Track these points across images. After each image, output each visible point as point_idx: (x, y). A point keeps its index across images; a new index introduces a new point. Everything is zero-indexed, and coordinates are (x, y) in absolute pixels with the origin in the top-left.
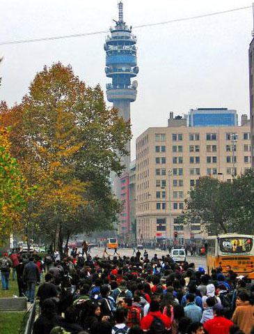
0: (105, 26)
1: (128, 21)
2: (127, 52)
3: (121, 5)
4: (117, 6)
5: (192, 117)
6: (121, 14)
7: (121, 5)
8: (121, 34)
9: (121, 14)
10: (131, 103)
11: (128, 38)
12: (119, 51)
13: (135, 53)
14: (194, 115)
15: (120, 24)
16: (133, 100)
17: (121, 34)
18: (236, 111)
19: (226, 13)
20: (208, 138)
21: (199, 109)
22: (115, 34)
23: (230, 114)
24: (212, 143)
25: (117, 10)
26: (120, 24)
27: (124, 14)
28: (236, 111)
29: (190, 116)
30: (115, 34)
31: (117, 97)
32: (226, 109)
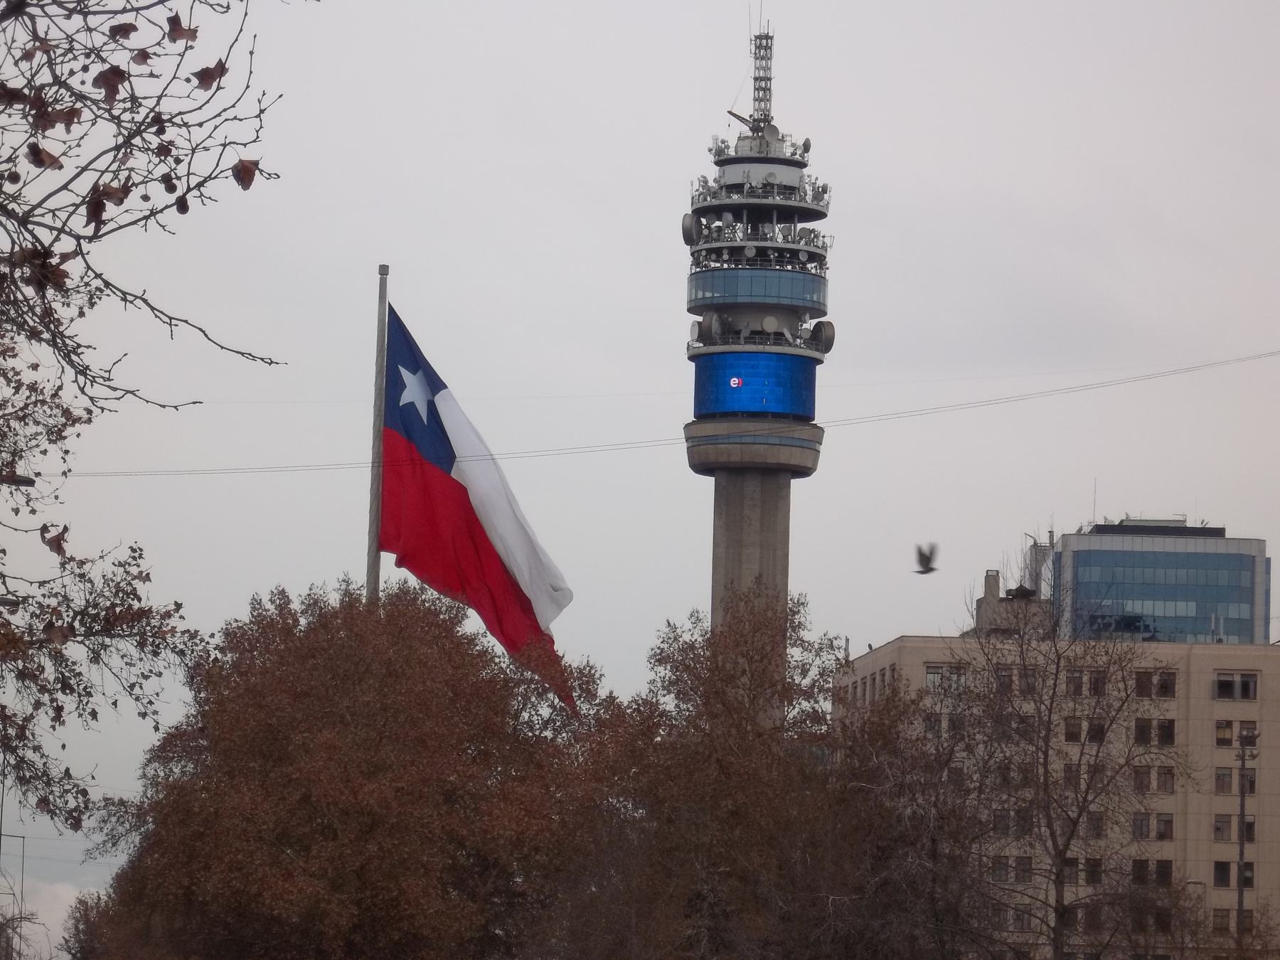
0: (685, 172)
1: (791, 124)
2: (787, 255)
3: (763, 45)
4: (745, 50)
5: (1068, 561)
6: (763, 86)
7: (763, 45)
8: (757, 174)
9: (763, 86)
10: (795, 483)
11: (789, 190)
12: (751, 253)
13: (819, 258)
14: (1077, 554)
15: (761, 125)
16: (804, 472)
17: (757, 174)
18: (1261, 543)
19: (755, 407)
20: (1224, 689)
21: (1100, 530)
22: (735, 174)
23: (1239, 557)
24: (1235, 710)
25: (747, 67)
26: (761, 125)
27: (774, 85)
28: (1261, 543)
29: (1058, 558)
30: (735, 174)
31: (734, 454)
32: (1219, 533)
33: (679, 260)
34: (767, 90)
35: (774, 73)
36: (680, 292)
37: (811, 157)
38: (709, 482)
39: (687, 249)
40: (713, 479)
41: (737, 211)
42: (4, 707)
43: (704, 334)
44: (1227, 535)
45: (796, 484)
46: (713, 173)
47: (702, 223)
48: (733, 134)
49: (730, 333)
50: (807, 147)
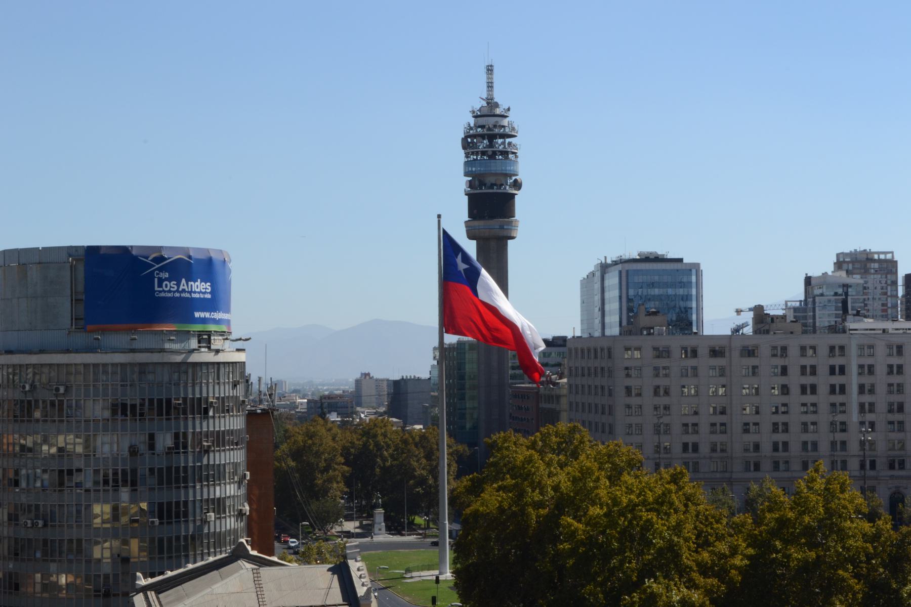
0: (462, 120)
3: (490, 70)
6: (490, 86)
7: (490, 70)
8: (491, 121)
9: (490, 86)
17: (491, 121)
22: (482, 121)
25: (484, 78)
26: (491, 104)
27: (495, 85)
30: (482, 121)
32: (681, 260)
33: (460, 156)
34: (492, 87)
35: (494, 80)
36: (461, 169)
37: (510, 114)
38: (474, 242)
39: (463, 152)
40: (425, 375)
41: (483, 136)
42: (131, 290)
43: (471, 184)
44: (685, 261)
45: (510, 242)
46: (472, 122)
47: (468, 143)
48: (479, 104)
49: (482, 184)
50: (509, 109)
